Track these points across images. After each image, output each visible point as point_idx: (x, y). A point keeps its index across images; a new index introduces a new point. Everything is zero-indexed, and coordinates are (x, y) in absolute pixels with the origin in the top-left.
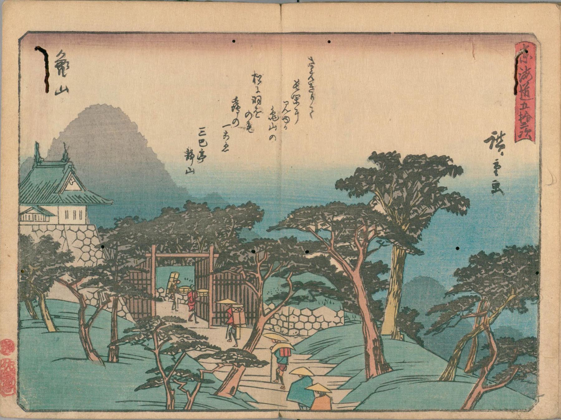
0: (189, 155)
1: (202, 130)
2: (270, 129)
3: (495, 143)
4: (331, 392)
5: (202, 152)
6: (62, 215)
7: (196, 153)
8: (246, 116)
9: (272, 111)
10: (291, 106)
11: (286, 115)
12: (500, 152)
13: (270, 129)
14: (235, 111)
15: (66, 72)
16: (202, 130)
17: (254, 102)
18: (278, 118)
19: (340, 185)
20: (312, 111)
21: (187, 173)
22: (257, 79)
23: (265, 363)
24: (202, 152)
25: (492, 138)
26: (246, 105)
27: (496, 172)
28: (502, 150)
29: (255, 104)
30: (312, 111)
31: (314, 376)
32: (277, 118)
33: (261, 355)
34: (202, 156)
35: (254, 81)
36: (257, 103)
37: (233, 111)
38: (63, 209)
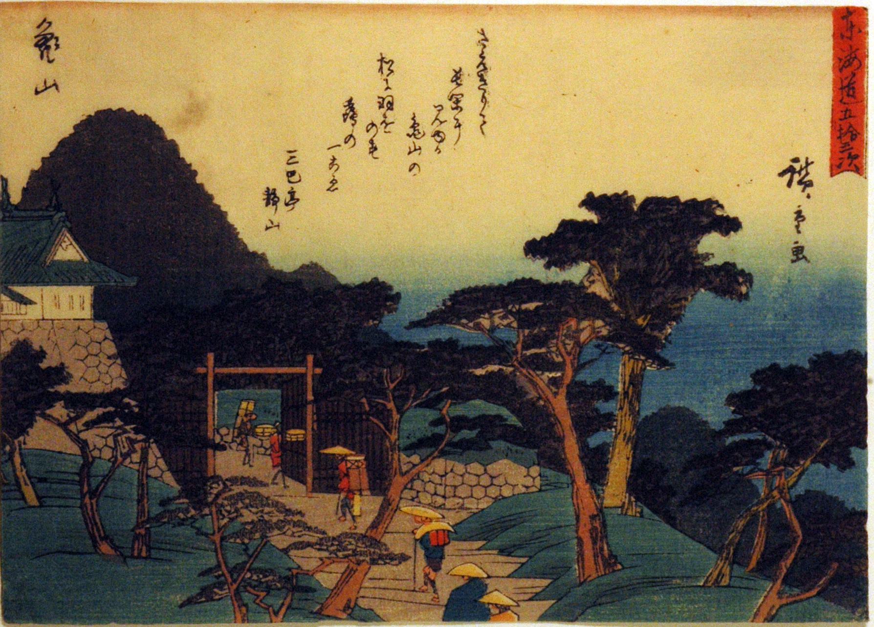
0: (271, 197)
1: (292, 155)
2: (410, 153)
3: (797, 177)
4: (518, 606)
5: (292, 193)
6: (48, 303)
7: (283, 194)
8: (368, 131)
9: (413, 122)
10: (448, 114)
11: (440, 128)
12: (805, 194)
13: (410, 153)
14: (349, 121)
15: (53, 53)
16: (292, 155)
17: (381, 107)
18: (424, 135)
19: (533, 248)
20: (485, 123)
21: (267, 228)
22: (386, 67)
23: (403, 558)
24: (292, 193)
25: (791, 170)
26: (367, 111)
27: (797, 227)
28: (809, 190)
29: (383, 110)
30: (485, 123)
31: (489, 577)
32: (422, 133)
33: (396, 543)
34: (293, 199)
35: (381, 69)
36: (386, 108)
37: (345, 120)
38: (50, 291)
